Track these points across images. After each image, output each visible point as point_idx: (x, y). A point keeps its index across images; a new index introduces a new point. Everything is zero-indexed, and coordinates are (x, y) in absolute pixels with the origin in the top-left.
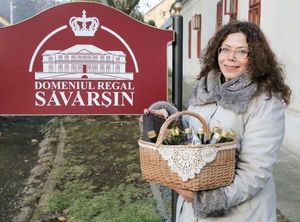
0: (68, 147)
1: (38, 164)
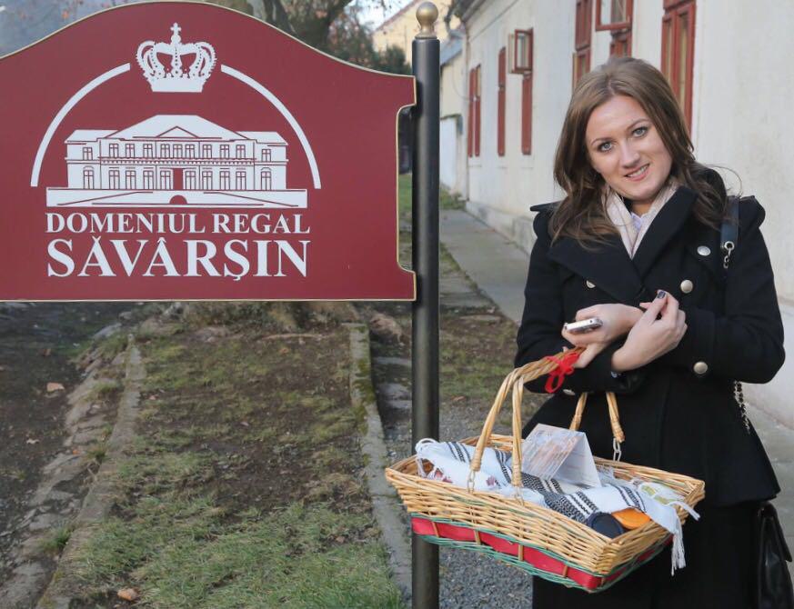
0: (147, 402)
1: (64, 450)
